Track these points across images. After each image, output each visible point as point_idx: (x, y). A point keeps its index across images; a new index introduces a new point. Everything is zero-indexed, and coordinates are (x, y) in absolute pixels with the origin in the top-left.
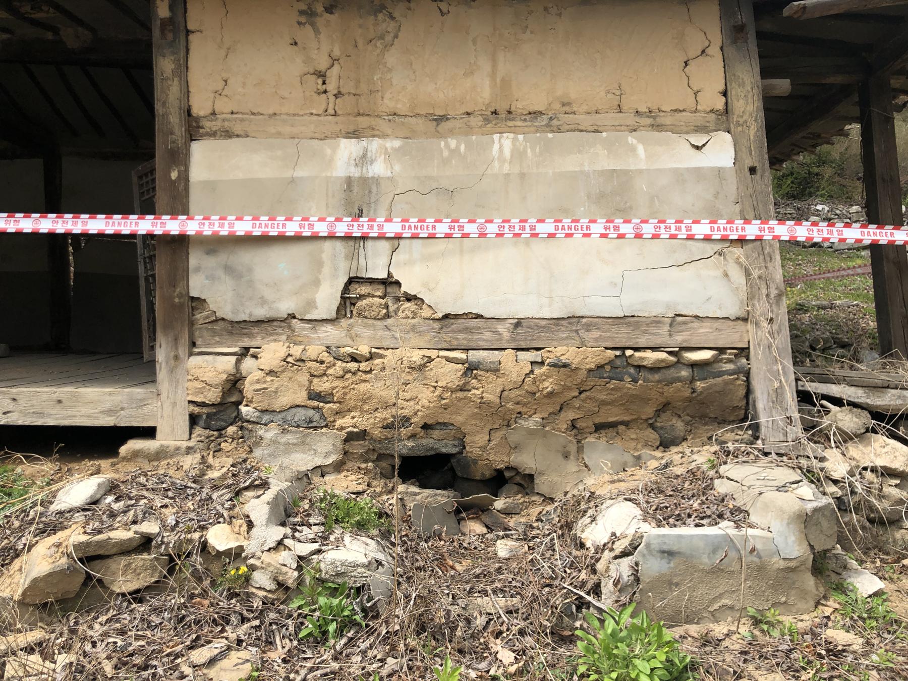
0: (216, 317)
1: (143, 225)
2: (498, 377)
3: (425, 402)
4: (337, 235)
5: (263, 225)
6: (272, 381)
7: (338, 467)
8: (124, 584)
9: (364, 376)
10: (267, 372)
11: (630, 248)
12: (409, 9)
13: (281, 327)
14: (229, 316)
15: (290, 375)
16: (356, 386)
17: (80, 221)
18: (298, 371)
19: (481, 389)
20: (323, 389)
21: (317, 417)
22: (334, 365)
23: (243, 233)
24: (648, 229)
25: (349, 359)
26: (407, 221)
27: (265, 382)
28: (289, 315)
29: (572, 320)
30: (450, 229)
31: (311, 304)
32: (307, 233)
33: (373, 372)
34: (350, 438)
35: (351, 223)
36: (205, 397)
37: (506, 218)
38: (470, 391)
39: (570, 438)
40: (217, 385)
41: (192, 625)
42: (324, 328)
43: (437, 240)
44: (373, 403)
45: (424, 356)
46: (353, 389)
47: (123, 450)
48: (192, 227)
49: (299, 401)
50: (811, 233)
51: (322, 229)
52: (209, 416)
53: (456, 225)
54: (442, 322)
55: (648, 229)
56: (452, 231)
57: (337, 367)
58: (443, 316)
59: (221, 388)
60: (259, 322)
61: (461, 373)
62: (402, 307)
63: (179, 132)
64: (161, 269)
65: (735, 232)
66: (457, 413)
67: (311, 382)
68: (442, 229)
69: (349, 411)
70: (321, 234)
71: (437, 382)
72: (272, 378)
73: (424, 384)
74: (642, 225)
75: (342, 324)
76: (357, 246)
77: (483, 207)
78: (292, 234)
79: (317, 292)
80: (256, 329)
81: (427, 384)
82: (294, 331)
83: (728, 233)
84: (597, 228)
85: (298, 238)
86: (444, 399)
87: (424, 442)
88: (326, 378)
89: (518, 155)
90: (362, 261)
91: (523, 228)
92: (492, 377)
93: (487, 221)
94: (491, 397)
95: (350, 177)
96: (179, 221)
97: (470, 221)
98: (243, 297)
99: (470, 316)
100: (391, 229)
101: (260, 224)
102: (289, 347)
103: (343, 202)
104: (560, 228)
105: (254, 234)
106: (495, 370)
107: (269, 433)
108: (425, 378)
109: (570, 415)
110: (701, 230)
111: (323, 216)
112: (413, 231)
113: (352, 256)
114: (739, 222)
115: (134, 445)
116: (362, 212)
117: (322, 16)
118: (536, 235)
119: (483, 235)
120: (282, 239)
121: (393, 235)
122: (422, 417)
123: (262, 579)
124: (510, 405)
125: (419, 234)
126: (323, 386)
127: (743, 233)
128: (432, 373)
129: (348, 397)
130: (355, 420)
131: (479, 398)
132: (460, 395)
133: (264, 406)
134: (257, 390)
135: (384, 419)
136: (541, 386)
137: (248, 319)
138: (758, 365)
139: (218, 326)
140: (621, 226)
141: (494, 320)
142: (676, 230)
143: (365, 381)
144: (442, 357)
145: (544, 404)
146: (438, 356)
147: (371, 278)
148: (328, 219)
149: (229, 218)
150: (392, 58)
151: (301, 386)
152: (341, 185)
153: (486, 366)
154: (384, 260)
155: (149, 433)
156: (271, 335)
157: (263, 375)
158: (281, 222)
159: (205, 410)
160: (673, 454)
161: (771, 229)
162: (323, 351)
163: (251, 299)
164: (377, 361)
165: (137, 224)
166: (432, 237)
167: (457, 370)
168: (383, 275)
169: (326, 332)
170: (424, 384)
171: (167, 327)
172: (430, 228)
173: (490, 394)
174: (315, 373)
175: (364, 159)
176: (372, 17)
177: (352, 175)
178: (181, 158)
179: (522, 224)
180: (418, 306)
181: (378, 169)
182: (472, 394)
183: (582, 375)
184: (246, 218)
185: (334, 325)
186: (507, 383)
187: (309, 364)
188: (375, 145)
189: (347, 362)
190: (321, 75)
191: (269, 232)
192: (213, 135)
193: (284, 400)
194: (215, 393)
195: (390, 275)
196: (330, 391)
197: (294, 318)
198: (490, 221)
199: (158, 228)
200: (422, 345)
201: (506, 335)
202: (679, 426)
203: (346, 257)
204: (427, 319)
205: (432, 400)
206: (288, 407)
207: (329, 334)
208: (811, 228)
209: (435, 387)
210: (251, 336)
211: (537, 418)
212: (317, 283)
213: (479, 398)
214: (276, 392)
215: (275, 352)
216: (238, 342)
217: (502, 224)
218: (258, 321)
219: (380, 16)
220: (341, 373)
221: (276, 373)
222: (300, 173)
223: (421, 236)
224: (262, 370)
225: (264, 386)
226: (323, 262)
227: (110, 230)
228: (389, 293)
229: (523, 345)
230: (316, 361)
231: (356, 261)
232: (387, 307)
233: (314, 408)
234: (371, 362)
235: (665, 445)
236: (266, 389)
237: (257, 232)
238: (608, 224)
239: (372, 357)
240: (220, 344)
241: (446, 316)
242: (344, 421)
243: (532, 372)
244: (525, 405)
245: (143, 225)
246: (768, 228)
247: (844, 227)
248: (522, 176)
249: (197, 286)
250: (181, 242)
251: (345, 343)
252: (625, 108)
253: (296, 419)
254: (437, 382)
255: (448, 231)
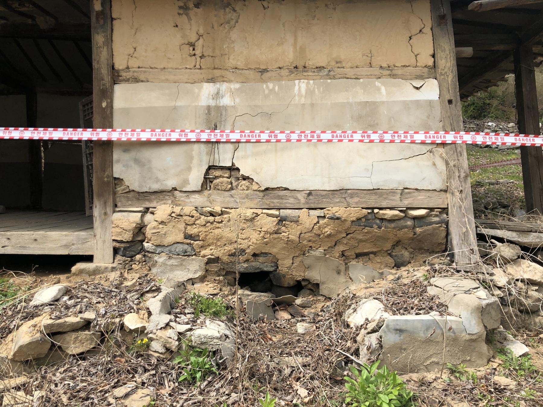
0: (129, 189)
1: (86, 135)
2: (298, 225)
3: (254, 240)
4: (202, 140)
5: (157, 135)
6: (163, 227)
7: (202, 279)
8: (74, 349)
9: (218, 225)
10: (160, 222)
11: (377, 148)
12: (245, 5)
13: (168, 195)
14: (137, 189)
15: (174, 224)
16: (213, 231)
17: (48, 132)
18: (178, 222)
19: (288, 233)
20: (193, 233)
21: (189, 249)
22: (200, 218)
23: (145, 140)
24: (387, 137)
25: (209, 215)
26: (243, 132)
27: (158, 228)
28: (173, 188)
29: (342, 191)
30: (269, 137)
31: (186, 182)
32: (183, 139)
33: (223, 222)
34: (210, 262)
35: (210, 133)
36: (123, 237)
37: (302, 131)
38: (281, 233)
39: (341, 262)
40: (130, 230)
41: (115, 373)
42: (194, 196)
43: (261, 143)
44: (223, 241)
45: (254, 213)
46: (211, 232)
47: (74, 269)
48: (115, 136)
49: (179, 240)
50: (485, 139)
51: (192, 137)
52: (125, 248)
53: (273, 134)
54: (264, 193)
55: (387, 137)
56: (271, 138)
57: (202, 219)
58: (265, 189)
59: (132, 232)
60: (155, 192)
61: (276, 223)
62: (241, 184)
63: (107, 79)
64: (96, 161)
65: (440, 139)
66: (273, 247)
67: (186, 228)
68: (264, 137)
69: (209, 245)
70: (192, 140)
71: (261, 228)
72: (163, 226)
73: (254, 230)
74: (384, 134)
75: (204, 194)
76: (213, 147)
77: (289, 124)
78: (175, 140)
79: (190, 174)
80: (153, 197)
81: (255, 230)
82: (176, 198)
83: (436, 139)
84: (357, 137)
85: (178, 142)
86: (266, 238)
87: (254, 264)
88: (195, 226)
89: (310, 92)
90: (216, 156)
91: (313, 137)
92: (294, 225)
93: (291, 132)
94: (294, 237)
95: (209, 106)
96: (107, 132)
97: (281, 132)
98: (145, 177)
99: (281, 189)
100: (234, 137)
101: (156, 134)
102: (173, 207)
103: (205, 121)
104: (335, 136)
105: (152, 140)
106: (296, 221)
107: (161, 259)
108: (254, 226)
109: (341, 248)
110: (419, 137)
111: (193, 129)
112: (247, 138)
113: (211, 153)
114: (442, 133)
115: (80, 266)
116: (216, 127)
117: (192, 9)
118: (321, 140)
119: (289, 140)
120: (169, 143)
121: (235, 141)
122: (253, 249)
123: (156, 346)
124: (305, 242)
125: (250, 140)
126: (193, 230)
127: (444, 139)
128: (258, 223)
129: (208, 237)
130: (212, 251)
131: (286, 238)
132: (275, 236)
133: (158, 242)
134: (154, 233)
135: (230, 251)
136: (324, 231)
137: (148, 191)
138: (453, 218)
139: (131, 195)
140: (372, 135)
141: (295, 191)
142: (404, 137)
143: (218, 228)
144: (264, 213)
145: (325, 242)
146: (262, 213)
147: (222, 166)
148: (196, 131)
149: (137, 130)
150: (234, 35)
151: (180, 231)
152: (204, 111)
153: (291, 219)
154: (230, 156)
155: (89, 259)
156: (162, 200)
157: (157, 224)
158: (168, 133)
159: (123, 245)
160: (403, 271)
161: (461, 137)
162: (193, 210)
163: (150, 178)
164: (225, 216)
165: (82, 134)
166: (258, 141)
167: (273, 221)
168: (229, 164)
169: (195, 198)
170: (254, 230)
171: (100, 196)
172: (257, 136)
173: (293, 235)
174: (189, 223)
175: (217, 95)
176: (223, 10)
177: (210, 105)
178: (108, 94)
179: (312, 134)
180: (250, 183)
181: (226, 101)
182: (282, 236)
183: (348, 224)
184: (147, 130)
185: (200, 194)
186: (303, 229)
187: (185, 218)
188: (224, 86)
189: (208, 216)
190: (192, 45)
191: (161, 139)
192: (127, 80)
193: (170, 239)
194: (129, 235)
195: (233, 164)
196: (197, 234)
197: (176, 190)
198: (293, 132)
199: (95, 136)
200: (252, 206)
201: (303, 200)
202: (406, 254)
203: (207, 154)
204: (255, 191)
205: (258, 239)
206: (172, 243)
207: (196, 200)
208: (485, 136)
209: (260, 231)
210: (150, 201)
211: (321, 250)
212: (189, 169)
213: (286, 238)
214: (165, 234)
215: (164, 210)
216: (142, 204)
217: (300, 134)
218: (155, 192)
219: (227, 10)
220: (204, 223)
221: (165, 223)
222: (179, 103)
223: (252, 141)
224: (157, 221)
225: (158, 231)
226: (193, 157)
227: (66, 138)
228: (232, 175)
229: (313, 206)
230: (189, 216)
231: (213, 156)
232: (231, 183)
233: (188, 244)
234: (222, 216)
235: (398, 266)
236: (159, 232)
237: (154, 139)
238: (363, 134)
239: (222, 213)
240: (131, 205)
241: (267, 189)
242: (206, 252)
243: (318, 222)
244: (314, 242)
245: (86, 135)
246: (460, 136)
247: (505, 135)
248: (312, 105)
249: (118, 171)
250: (108, 145)
251: (206, 205)
252: (374, 64)
253: (177, 250)
254: (261, 228)
255: (268, 138)
